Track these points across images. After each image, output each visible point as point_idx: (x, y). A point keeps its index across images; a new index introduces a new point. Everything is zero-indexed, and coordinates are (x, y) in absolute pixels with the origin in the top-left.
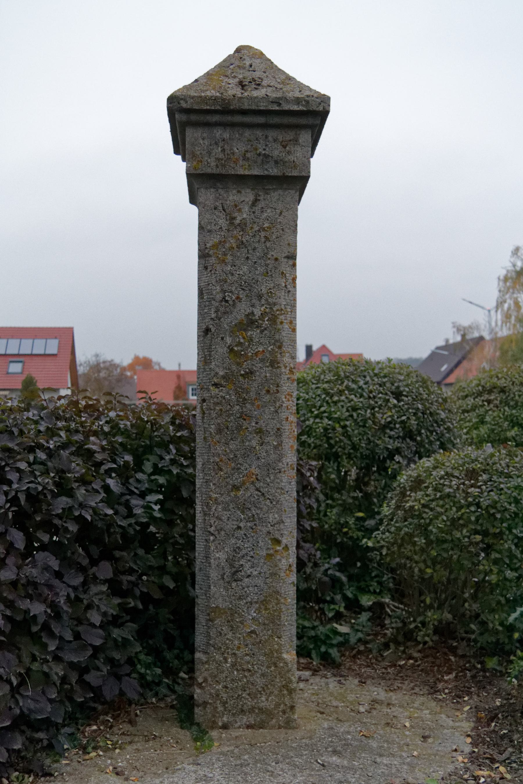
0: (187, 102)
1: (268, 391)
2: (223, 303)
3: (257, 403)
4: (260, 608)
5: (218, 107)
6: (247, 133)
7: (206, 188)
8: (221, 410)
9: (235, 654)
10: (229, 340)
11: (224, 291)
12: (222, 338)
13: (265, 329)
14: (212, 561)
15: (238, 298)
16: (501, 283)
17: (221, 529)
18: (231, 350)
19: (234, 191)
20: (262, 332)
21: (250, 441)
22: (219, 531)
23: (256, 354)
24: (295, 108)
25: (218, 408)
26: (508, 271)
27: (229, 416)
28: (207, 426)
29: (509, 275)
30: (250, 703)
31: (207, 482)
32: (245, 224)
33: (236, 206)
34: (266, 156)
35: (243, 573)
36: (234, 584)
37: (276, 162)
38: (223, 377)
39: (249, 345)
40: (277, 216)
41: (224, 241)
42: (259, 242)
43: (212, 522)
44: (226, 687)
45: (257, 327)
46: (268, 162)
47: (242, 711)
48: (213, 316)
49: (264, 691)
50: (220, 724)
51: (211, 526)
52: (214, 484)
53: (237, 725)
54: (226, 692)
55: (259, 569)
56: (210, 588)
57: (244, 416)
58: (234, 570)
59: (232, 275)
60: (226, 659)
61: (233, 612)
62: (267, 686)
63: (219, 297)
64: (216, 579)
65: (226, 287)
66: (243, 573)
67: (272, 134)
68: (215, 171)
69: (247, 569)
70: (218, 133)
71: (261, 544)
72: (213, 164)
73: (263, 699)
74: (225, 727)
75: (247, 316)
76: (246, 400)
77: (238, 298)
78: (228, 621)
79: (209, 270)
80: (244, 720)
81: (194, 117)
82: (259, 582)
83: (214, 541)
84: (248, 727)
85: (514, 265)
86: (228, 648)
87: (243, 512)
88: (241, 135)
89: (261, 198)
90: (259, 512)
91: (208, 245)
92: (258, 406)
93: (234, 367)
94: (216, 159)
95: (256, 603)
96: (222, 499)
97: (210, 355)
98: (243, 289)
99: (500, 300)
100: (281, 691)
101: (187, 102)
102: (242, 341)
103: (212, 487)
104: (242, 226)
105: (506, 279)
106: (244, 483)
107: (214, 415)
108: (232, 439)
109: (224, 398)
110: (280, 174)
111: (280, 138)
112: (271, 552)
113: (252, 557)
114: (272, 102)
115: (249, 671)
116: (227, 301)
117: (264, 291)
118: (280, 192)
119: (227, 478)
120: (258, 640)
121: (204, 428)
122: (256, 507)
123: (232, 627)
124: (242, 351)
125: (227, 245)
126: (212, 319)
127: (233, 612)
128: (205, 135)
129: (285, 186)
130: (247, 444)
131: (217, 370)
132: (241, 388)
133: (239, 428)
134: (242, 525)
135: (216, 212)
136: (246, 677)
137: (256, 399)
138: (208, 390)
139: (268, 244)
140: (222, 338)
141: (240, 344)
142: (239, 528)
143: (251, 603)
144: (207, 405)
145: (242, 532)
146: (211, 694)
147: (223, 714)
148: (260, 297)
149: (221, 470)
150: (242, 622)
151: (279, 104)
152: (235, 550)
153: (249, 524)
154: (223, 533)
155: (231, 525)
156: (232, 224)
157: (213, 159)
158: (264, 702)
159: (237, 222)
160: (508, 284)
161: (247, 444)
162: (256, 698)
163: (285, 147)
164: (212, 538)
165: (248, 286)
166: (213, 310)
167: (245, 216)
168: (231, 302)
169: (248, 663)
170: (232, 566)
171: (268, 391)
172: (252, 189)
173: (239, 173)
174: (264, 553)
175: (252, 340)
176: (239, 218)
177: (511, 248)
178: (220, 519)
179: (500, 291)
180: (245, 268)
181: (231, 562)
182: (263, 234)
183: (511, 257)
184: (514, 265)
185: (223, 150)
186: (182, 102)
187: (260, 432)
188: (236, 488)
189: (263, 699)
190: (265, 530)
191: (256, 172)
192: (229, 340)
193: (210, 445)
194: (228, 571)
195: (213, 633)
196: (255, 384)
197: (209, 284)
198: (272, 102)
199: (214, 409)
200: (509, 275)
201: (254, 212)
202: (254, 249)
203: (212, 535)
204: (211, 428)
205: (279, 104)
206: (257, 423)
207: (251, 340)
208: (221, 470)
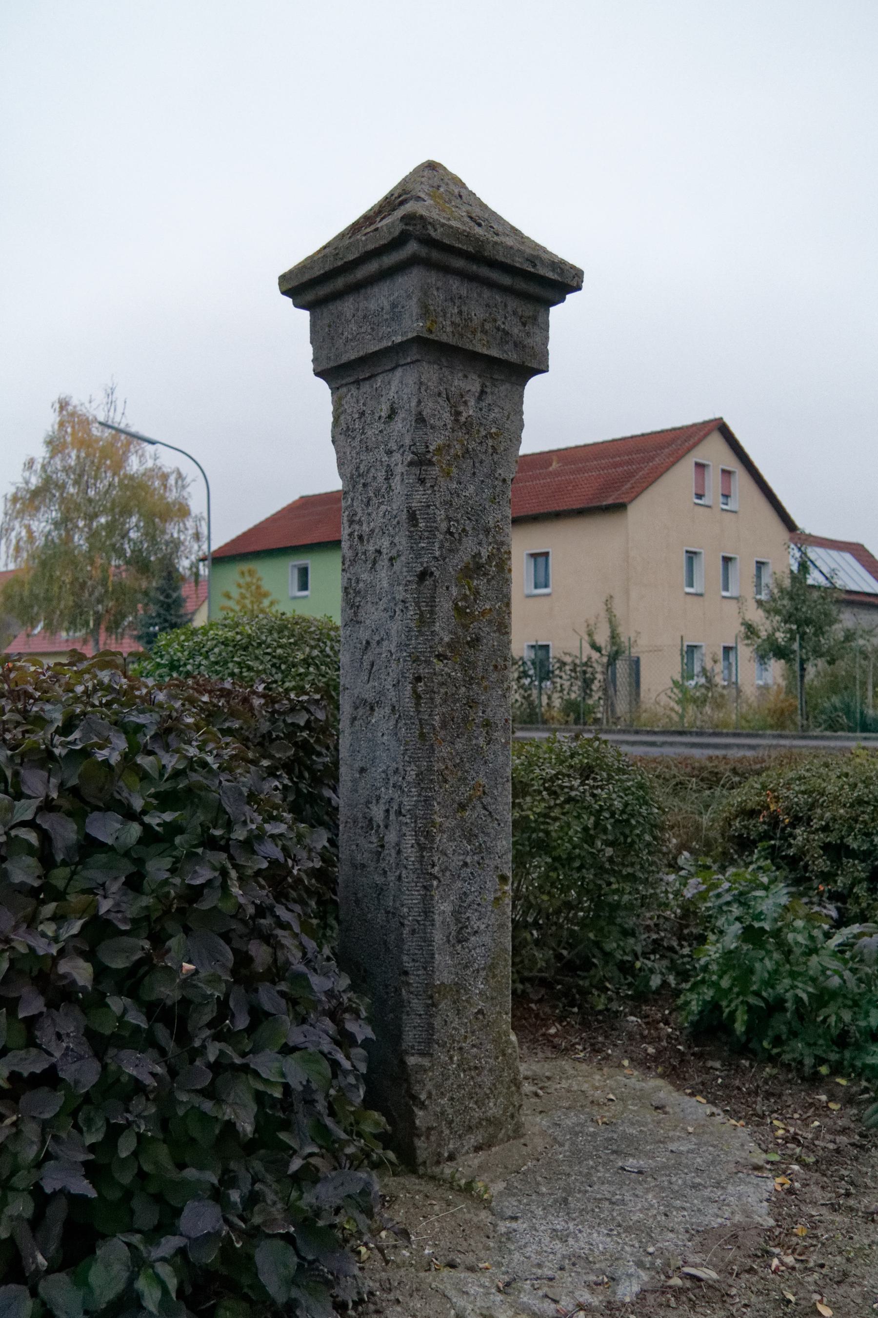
0: (436, 230)
1: (496, 667)
2: (448, 537)
3: (485, 683)
4: (487, 975)
5: (471, 249)
6: (487, 293)
7: (429, 362)
8: (446, 693)
9: (461, 1049)
10: (454, 591)
11: (449, 519)
12: (447, 588)
13: (493, 578)
14: (436, 917)
15: (464, 530)
16: (9, 504)
17: (447, 869)
18: (456, 608)
19: (460, 375)
20: (489, 581)
21: (477, 738)
22: (443, 871)
23: (483, 613)
24: (551, 275)
25: (442, 691)
26: (17, 488)
27: (454, 702)
28: (426, 717)
29: (19, 495)
30: (477, 1114)
31: (425, 801)
32: (472, 424)
33: (462, 396)
34: (506, 333)
35: (469, 930)
36: (459, 947)
37: (516, 345)
38: (449, 645)
39: (475, 600)
40: (505, 419)
41: (449, 446)
42: (486, 452)
43: (435, 859)
44: (452, 1099)
45: (485, 574)
46: (507, 342)
47: (470, 1127)
48: (437, 554)
49: (492, 1092)
50: (446, 1155)
51: (433, 866)
52: (439, 803)
53: (464, 1151)
54: (453, 1107)
55: (486, 921)
56: (433, 958)
57: (471, 703)
58: (460, 925)
59: (458, 496)
60: (451, 1058)
61: (459, 987)
62: (494, 1085)
63: (444, 526)
64: (440, 942)
65: (451, 513)
66: (469, 930)
67: (513, 303)
68: (452, 341)
69: (476, 924)
70: (456, 285)
71: (489, 885)
72: (449, 329)
73: (491, 1104)
74: (451, 1158)
75: (474, 557)
76: (472, 678)
77: (464, 530)
78: (454, 1003)
79: (428, 485)
80: (472, 1140)
81: (435, 255)
82: (486, 939)
83: (438, 887)
84: (478, 1149)
85: (27, 482)
86: (454, 1041)
87: (469, 842)
88: (479, 295)
89: (488, 390)
90: (486, 839)
91: (432, 448)
92: (485, 688)
93: (460, 631)
94: (452, 323)
95: (484, 969)
96: (447, 825)
97: (432, 612)
98: (469, 519)
99: (6, 526)
100: (509, 1087)
101: (436, 230)
102: (468, 593)
103: (437, 808)
104: (468, 426)
105: (15, 499)
106: (470, 799)
107: (438, 701)
108: (458, 736)
109: (449, 675)
110: (518, 361)
111: (519, 310)
112: (499, 894)
113: (479, 904)
114: (527, 260)
115: (476, 1068)
116: (451, 534)
117: (491, 524)
118: (507, 386)
119: (453, 792)
120: (485, 1023)
121: (420, 720)
122: (483, 832)
123: (458, 1010)
124: (467, 607)
125: (452, 451)
126: (435, 557)
127: (459, 987)
128: (440, 284)
129: (513, 379)
130: (474, 742)
131: (442, 633)
132: (467, 661)
133: (465, 719)
134: (468, 860)
135: (439, 400)
136: (472, 1078)
137: (483, 677)
138: (428, 662)
139: (496, 457)
140: (447, 588)
141: (465, 598)
142: (466, 864)
143: (478, 971)
144: (426, 685)
145: (469, 870)
146: (435, 1114)
147: (449, 1139)
148: (487, 531)
149: (446, 781)
150: (467, 1001)
151: (535, 266)
152: (461, 898)
153: (476, 858)
154: (448, 874)
155: (456, 861)
156: (457, 421)
157: (448, 323)
158: (493, 1109)
159: (463, 419)
160: (18, 506)
161: (474, 742)
162: (483, 1104)
163: (524, 324)
164: (435, 883)
165: (476, 514)
166: (437, 545)
167: (471, 413)
168: (456, 536)
169: (475, 1057)
170: (458, 921)
171: (496, 667)
172: (480, 376)
173: (476, 349)
174: (492, 897)
175: (478, 593)
176: (465, 414)
177: (24, 459)
178: (446, 855)
179: (6, 514)
180: (472, 488)
181: (457, 913)
182: (490, 442)
183: (24, 470)
184: (27, 482)
185: (460, 313)
186: (429, 227)
187: (487, 725)
188: (462, 807)
189: (491, 1104)
190: (492, 864)
191: (495, 353)
192: (454, 591)
193: (432, 745)
194: (454, 928)
195: (437, 1022)
196: (482, 657)
197: (429, 506)
198: (527, 260)
199: (439, 693)
200: (19, 495)
201: (481, 409)
202: (481, 462)
203: (436, 878)
204: (434, 720)
205: (535, 266)
206: (484, 712)
207: (477, 593)
208: (446, 781)
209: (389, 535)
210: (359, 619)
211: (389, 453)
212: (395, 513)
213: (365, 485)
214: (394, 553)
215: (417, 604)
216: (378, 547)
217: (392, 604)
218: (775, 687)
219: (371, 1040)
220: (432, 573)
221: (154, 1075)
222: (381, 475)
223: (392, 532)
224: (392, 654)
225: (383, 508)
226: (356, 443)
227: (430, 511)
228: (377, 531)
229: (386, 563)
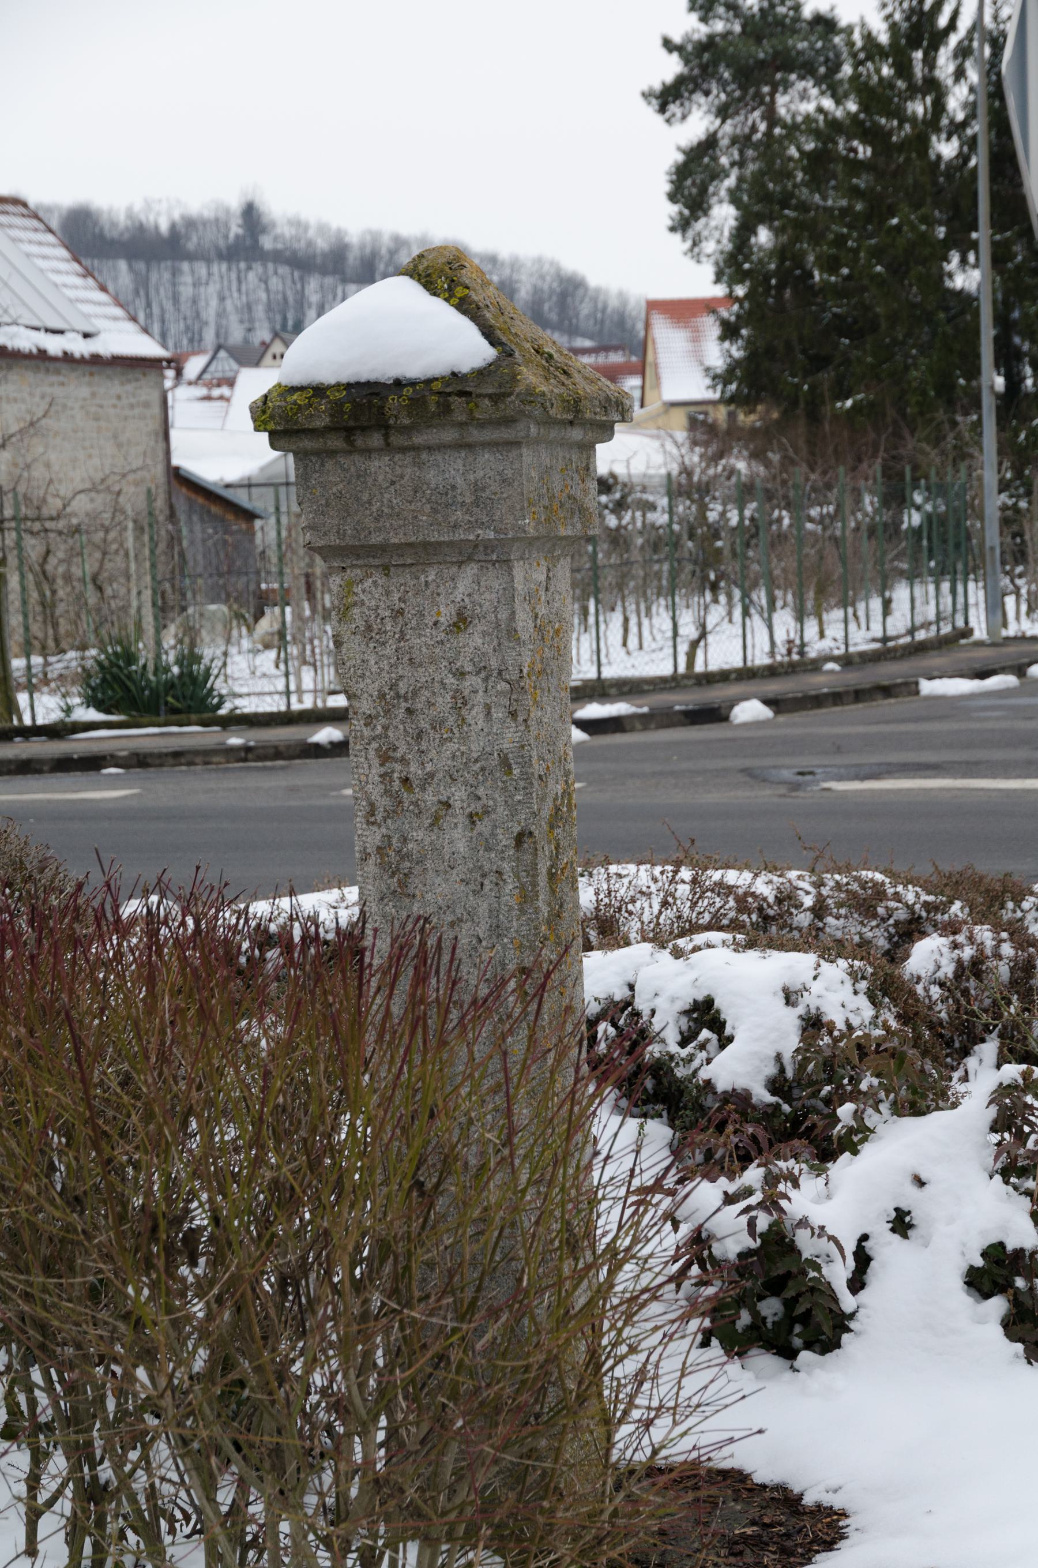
209: (466, 783)
210: (411, 891)
211: (461, 674)
212: (475, 755)
213: (409, 711)
214: (476, 807)
215: (517, 876)
216: (444, 799)
217: (477, 875)
218: (821, 118)
219: (1009, 1115)
220: (531, 833)
221: (651, 1255)
222: (444, 702)
223: (472, 780)
224: (480, 941)
225: (452, 747)
226: (389, 651)
227: (525, 752)
228: (440, 775)
229: (462, 820)
